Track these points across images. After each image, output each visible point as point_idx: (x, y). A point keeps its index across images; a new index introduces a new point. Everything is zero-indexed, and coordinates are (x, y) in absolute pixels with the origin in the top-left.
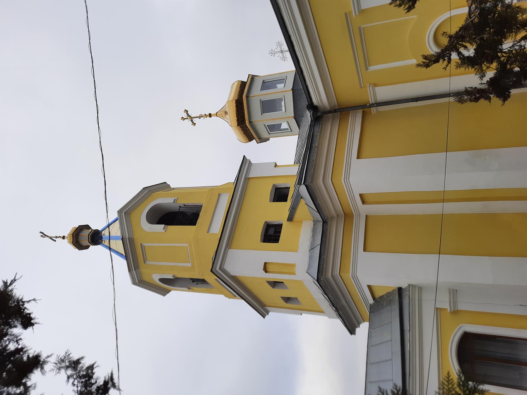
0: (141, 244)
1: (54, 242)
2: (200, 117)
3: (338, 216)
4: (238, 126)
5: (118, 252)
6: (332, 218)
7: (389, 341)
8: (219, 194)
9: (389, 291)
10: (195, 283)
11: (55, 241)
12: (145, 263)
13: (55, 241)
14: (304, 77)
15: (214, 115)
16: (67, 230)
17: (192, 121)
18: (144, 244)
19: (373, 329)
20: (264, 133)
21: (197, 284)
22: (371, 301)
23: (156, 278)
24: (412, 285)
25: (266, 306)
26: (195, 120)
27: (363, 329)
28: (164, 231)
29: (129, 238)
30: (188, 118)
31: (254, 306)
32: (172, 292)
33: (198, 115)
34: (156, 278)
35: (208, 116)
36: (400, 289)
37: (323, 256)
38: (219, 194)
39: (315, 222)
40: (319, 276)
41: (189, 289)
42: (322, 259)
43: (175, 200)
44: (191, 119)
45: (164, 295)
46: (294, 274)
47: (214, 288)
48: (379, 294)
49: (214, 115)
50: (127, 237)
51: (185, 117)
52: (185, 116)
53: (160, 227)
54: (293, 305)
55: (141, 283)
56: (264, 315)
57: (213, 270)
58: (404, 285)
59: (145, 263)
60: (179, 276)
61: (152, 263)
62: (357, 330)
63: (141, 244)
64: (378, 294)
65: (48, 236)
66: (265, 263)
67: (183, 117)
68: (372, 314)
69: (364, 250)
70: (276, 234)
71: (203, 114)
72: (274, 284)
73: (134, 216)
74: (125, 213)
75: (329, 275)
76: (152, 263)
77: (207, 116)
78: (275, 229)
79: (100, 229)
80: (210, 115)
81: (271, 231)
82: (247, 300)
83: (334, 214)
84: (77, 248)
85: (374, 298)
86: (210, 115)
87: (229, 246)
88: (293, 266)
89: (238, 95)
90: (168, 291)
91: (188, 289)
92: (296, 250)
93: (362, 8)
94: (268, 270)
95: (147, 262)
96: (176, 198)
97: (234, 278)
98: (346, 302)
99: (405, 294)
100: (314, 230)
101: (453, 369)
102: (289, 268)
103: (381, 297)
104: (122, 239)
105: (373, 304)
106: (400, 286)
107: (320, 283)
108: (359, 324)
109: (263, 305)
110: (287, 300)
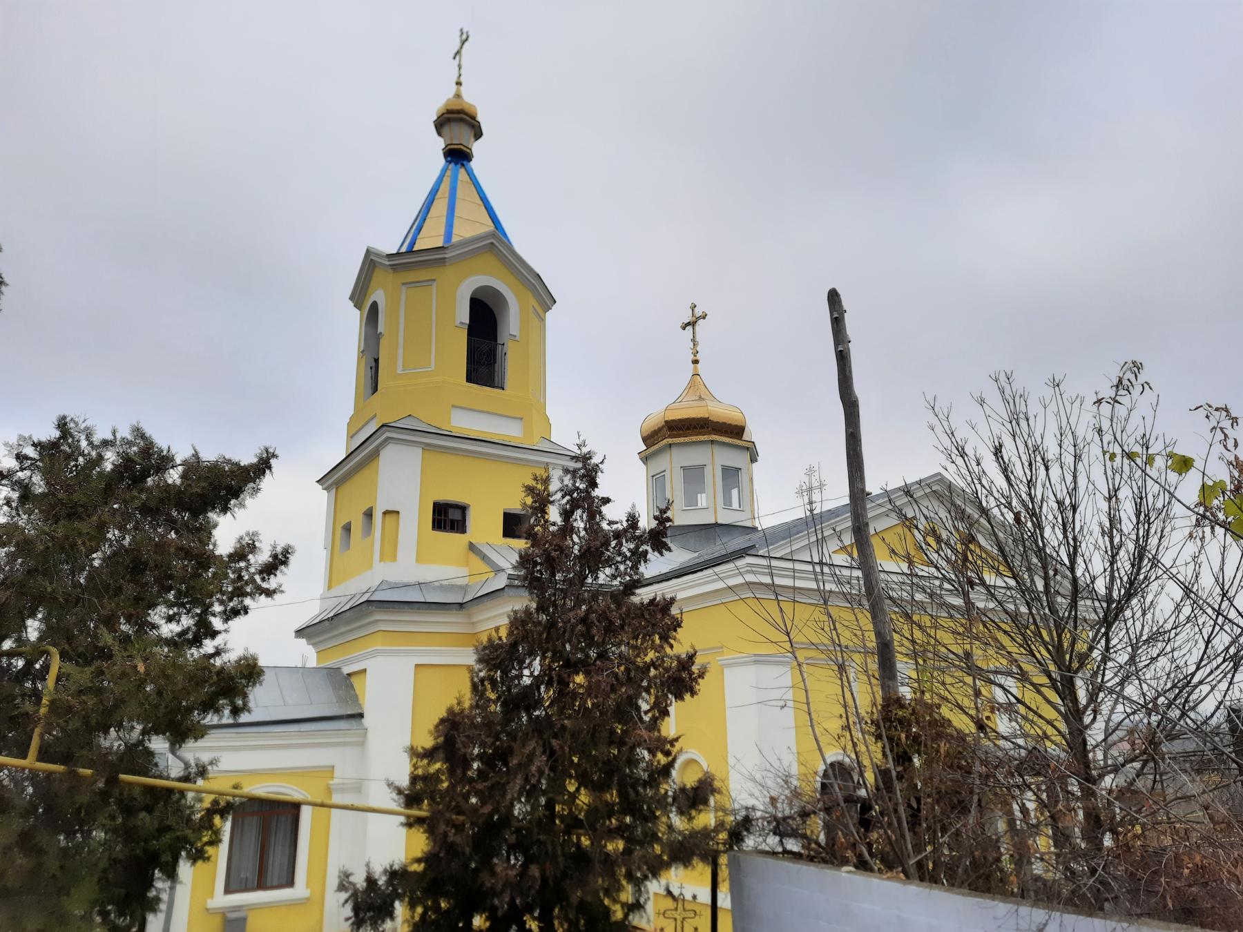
0: (434, 280)
1: (453, 55)
2: (694, 340)
3: (473, 624)
4: (666, 421)
5: (425, 219)
6: (470, 616)
7: (284, 701)
8: (521, 419)
9: (360, 697)
10: (373, 364)
11: (454, 58)
12: (403, 284)
13: (454, 58)
14: (661, 582)
15: (695, 369)
16: (472, 98)
17: (688, 324)
18: (435, 285)
19: (302, 675)
20: (662, 463)
21: (371, 368)
22: (346, 670)
23: (377, 295)
24: (366, 733)
25: (337, 489)
26: (689, 328)
27: (305, 654)
28: (457, 323)
29: (445, 258)
30: (694, 318)
31: (335, 471)
32: (357, 312)
33: (697, 339)
34: (377, 295)
35: (695, 358)
36: (361, 716)
37: (406, 607)
38: (521, 419)
39: (464, 589)
40: (375, 604)
41: (363, 352)
42: (402, 606)
43: (515, 336)
44: (692, 324)
45: (351, 298)
46: (382, 559)
47: (364, 401)
48: (355, 681)
49: (695, 369)
50: (446, 256)
51: (696, 310)
52: (698, 312)
53: (464, 315)
54: (339, 536)
55: (370, 264)
56: (322, 482)
57: (385, 428)
58: (367, 721)
59: (403, 284)
60: (383, 342)
61: (403, 298)
62: (303, 641)
63: (434, 280)
64: (354, 680)
65: (461, 47)
66: (398, 512)
67: (695, 306)
68: (325, 672)
69: (417, 666)
70: (448, 523)
71: (698, 349)
72: (369, 514)
73: (489, 260)
74: (492, 243)
75: (377, 617)
76: (403, 298)
77: (695, 356)
78: (457, 521)
79: (473, 164)
80: (696, 362)
81: (454, 515)
82: (344, 463)
83: (475, 619)
84: (438, 118)
85: (349, 675)
86: (696, 362)
87: (427, 448)
88: (394, 558)
89: (724, 423)
90: (358, 305)
91: (362, 349)
92: (419, 559)
93: (725, 670)
94: (387, 516)
95: (404, 288)
96: (518, 338)
97: (375, 454)
98: (342, 633)
99: (353, 723)
100: (452, 588)
101: (257, 786)
102: (390, 552)
103: (352, 686)
104: (443, 247)
105: (342, 673)
106: (366, 715)
107: (365, 605)
108: (314, 645)
109: (338, 484)
110: (347, 528)
